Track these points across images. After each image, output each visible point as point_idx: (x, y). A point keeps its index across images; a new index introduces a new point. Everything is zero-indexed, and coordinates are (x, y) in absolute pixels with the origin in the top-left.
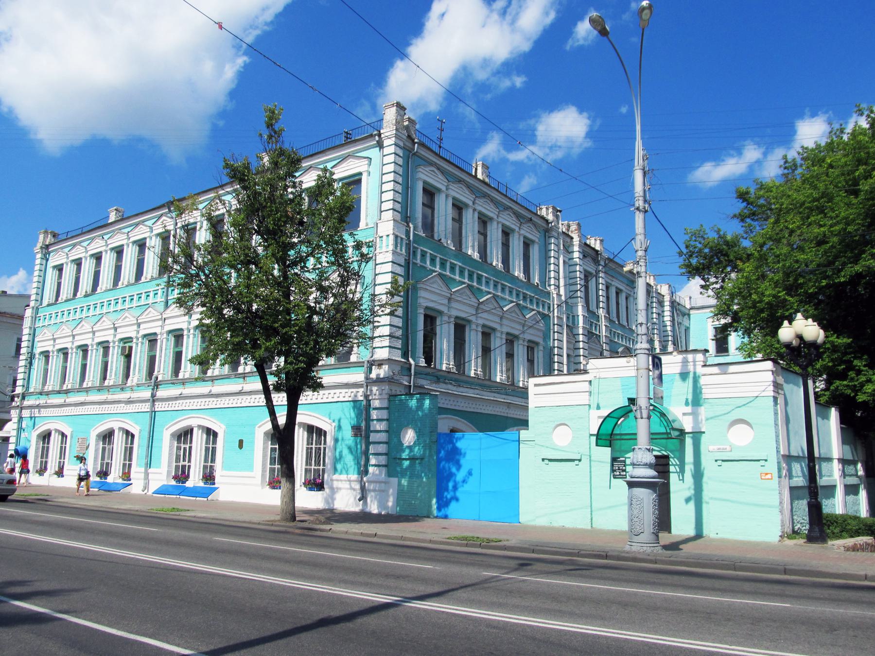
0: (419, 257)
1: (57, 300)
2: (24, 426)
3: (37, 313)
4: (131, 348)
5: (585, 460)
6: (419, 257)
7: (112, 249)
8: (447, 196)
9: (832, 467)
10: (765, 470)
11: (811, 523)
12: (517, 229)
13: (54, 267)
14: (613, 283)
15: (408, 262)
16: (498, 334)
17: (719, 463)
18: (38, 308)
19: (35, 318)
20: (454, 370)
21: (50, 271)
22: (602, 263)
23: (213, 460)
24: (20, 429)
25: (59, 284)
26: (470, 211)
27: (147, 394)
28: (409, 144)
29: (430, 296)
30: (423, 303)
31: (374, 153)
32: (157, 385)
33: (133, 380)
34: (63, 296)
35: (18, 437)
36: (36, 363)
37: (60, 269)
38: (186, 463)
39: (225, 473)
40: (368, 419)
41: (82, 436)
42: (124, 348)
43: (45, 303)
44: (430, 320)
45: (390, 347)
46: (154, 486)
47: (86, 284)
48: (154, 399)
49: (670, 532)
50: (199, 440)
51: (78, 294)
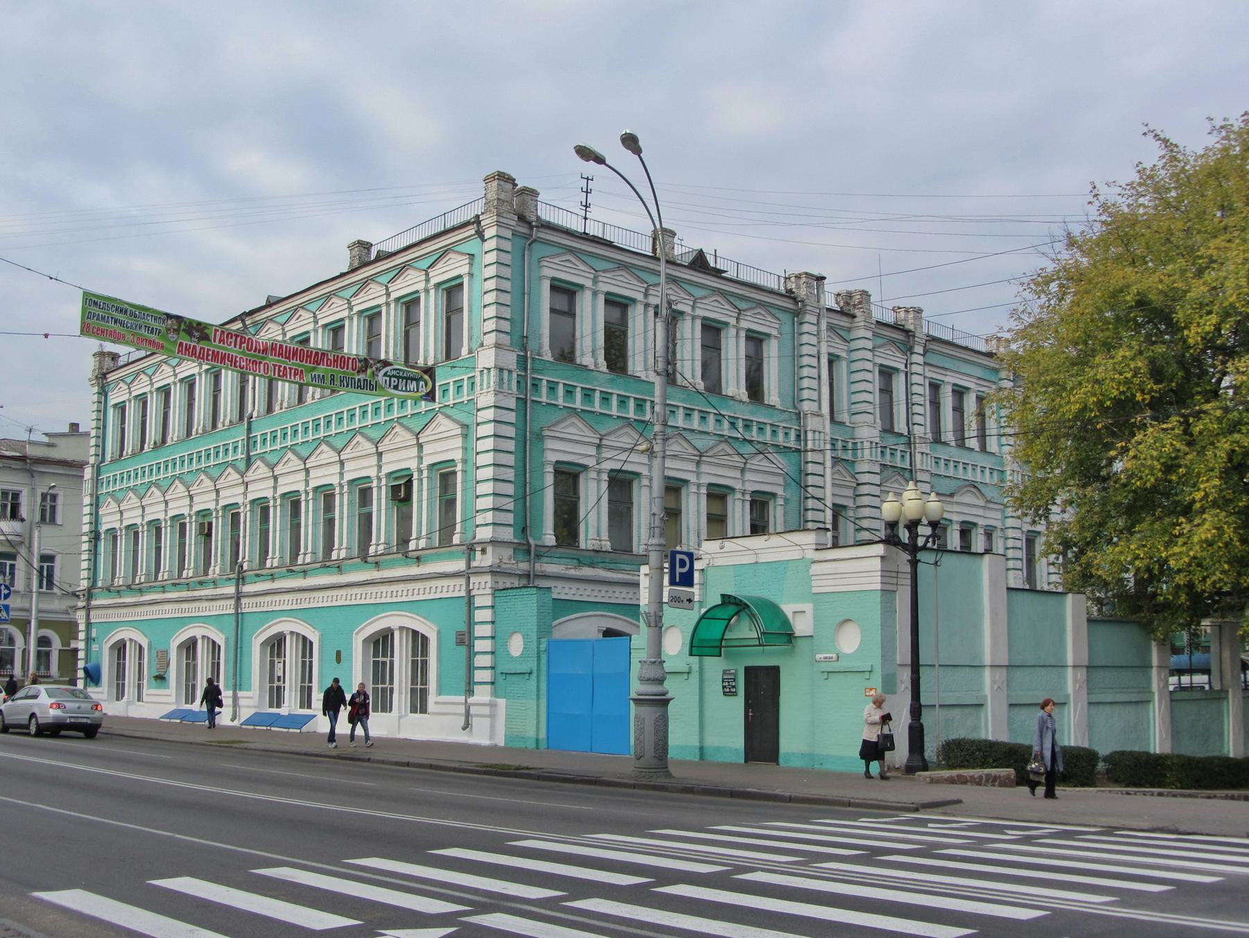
0: (544, 390)
1: (121, 455)
2: (94, 635)
3: (98, 474)
4: (210, 524)
5: (534, 675)
6: (544, 390)
7: (181, 380)
8: (595, 293)
9: (1065, 678)
10: (869, 684)
11: (911, 751)
12: (733, 321)
13: (115, 406)
14: (947, 379)
15: (522, 401)
16: (693, 489)
17: (825, 675)
18: (99, 468)
19: (97, 481)
20: (607, 546)
21: (111, 411)
22: (919, 349)
23: (310, 681)
24: (88, 640)
25: (123, 430)
26: (640, 308)
27: (231, 590)
28: (523, 229)
29: (567, 444)
30: (552, 457)
31: (473, 246)
32: (241, 579)
33: (215, 570)
34: (128, 449)
35: (88, 650)
36: (102, 545)
37: (121, 408)
38: (387, 685)
39: (153, 691)
40: (470, 623)
41: (162, 648)
42: (202, 525)
43: (108, 457)
44: (568, 476)
45: (494, 524)
46: (245, 714)
47: (153, 433)
48: (239, 596)
49: (778, 764)
50: (401, 647)
51: (146, 446)
